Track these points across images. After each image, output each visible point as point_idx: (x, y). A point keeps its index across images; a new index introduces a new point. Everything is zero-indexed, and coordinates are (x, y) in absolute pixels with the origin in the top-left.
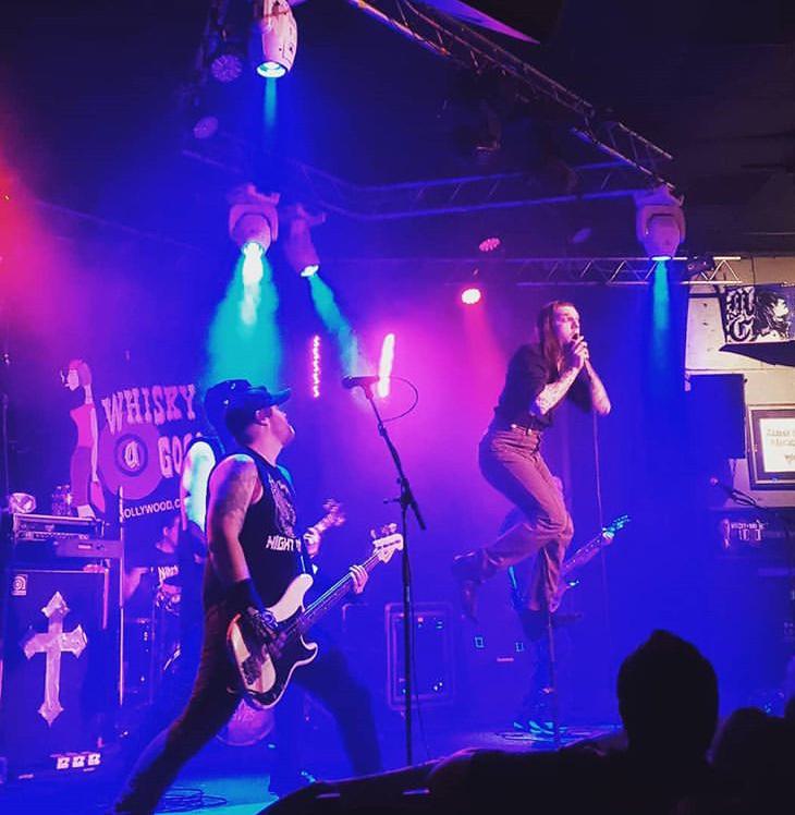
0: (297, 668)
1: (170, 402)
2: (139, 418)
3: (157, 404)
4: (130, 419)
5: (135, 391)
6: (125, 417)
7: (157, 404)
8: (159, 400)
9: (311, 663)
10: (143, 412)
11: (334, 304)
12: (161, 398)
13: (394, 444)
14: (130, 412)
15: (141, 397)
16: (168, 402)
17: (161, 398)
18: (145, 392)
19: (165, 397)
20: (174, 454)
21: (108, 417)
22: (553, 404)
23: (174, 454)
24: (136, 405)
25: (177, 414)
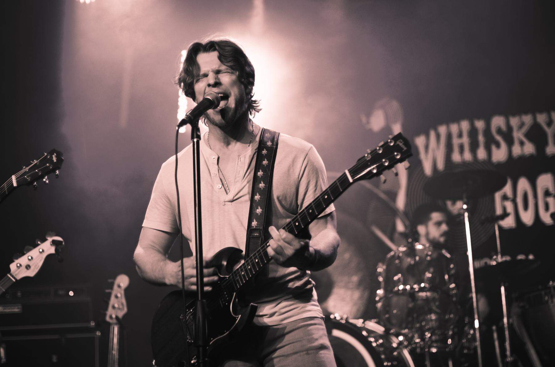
0: (234, 314)
1: (518, 135)
2: (468, 156)
3: (499, 138)
4: (456, 157)
5: (465, 125)
7: (499, 138)
8: (499, 131)
9: (234, 317)
10: (474, 147)
11: (187, 97)
13: (286, 347)
15: (473, 133)
17: (494, 148)
18: (480, 124)
19: (510, 129)
20: (520, 200)
21: (422, 156)
22: (41, 264)
23: (520, 200)
24: (465, 140)
25: (529, 149)
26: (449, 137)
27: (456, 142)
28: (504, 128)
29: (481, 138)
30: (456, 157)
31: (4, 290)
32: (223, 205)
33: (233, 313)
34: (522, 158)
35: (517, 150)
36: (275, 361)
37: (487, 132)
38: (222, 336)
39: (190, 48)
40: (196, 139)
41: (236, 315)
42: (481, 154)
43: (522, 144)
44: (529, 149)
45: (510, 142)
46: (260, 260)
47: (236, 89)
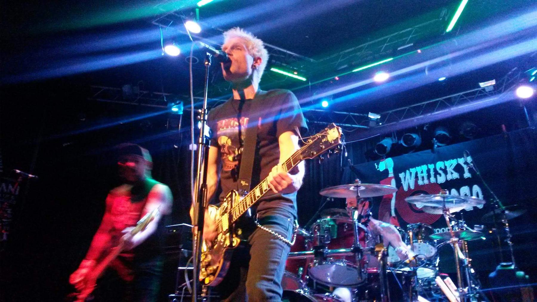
1: (449, 170)
3: (440, 172)
6: (416, 182)
7: (440, 172)
8: (441, 169)
10: (429, 176)
12: (438, 176)
14: (420, 178)
15: (428, 171)
16: (448, 169)
17: (438, 176)
19: (446, 167)
21: (403, 182)
24: (425, 174)
25: (456, 175)
26: (417, 173)
27: (420, 175)
28: (443, 167)
30: (420, 182)
32: (406, 252)
35: (449, 177)
37: (435, 170)
40: (181, 113)
41: (381, 153)
42: (433, 180)
43: (452, 173)
44: (456, 175)
47: (279, 180)
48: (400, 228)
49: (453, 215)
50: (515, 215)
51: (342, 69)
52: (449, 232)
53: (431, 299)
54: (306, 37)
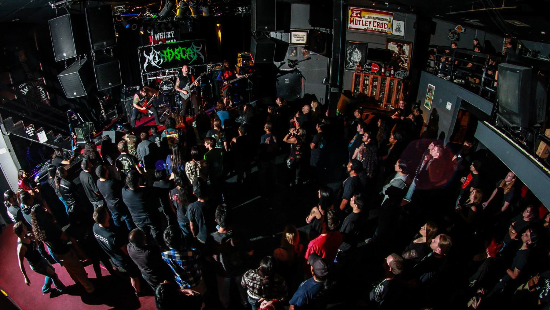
1: (168, 35)
2: (162, 38)
4: (161, 38)
5: (162, 33)
6: (160, 38)
10: (163, 36)
15: (163, 34)
21: (156, 37)
24: (162, 35)
25: (170, 36)
26: (160, 35)
27: (161, 36)
29: (164, 35)
30: (161, 38)
31: (406, 14)
33: (144, 163)
34: (169, 38)
35: (168, 37)
36: (327, 58)
38: (254, 199)
39: (519, 86)
44: (170, 36)
45: (167, 36)
46: (140, 71)
48: (212, 120)
49: (140, 222)
50: (96, 143)
51: (307, 295)
52: (160, 284)
53: (320, 259)
54: (223, 128)
